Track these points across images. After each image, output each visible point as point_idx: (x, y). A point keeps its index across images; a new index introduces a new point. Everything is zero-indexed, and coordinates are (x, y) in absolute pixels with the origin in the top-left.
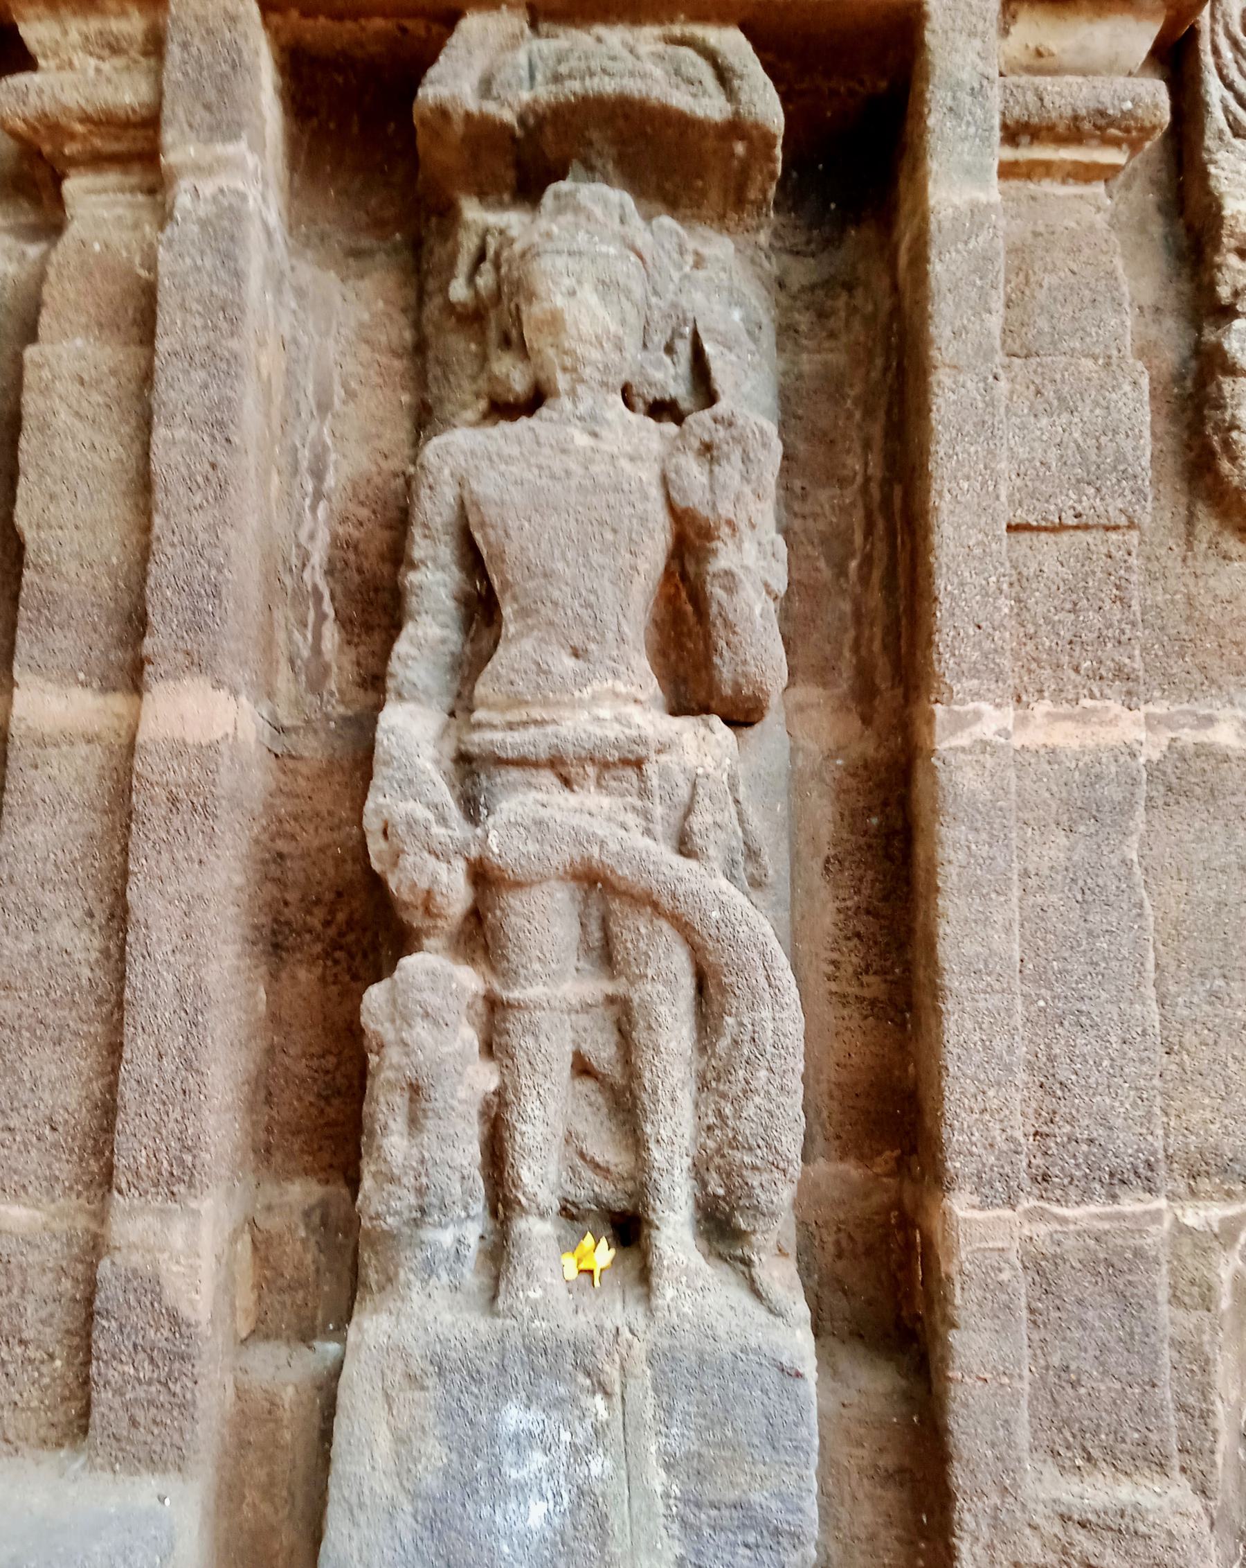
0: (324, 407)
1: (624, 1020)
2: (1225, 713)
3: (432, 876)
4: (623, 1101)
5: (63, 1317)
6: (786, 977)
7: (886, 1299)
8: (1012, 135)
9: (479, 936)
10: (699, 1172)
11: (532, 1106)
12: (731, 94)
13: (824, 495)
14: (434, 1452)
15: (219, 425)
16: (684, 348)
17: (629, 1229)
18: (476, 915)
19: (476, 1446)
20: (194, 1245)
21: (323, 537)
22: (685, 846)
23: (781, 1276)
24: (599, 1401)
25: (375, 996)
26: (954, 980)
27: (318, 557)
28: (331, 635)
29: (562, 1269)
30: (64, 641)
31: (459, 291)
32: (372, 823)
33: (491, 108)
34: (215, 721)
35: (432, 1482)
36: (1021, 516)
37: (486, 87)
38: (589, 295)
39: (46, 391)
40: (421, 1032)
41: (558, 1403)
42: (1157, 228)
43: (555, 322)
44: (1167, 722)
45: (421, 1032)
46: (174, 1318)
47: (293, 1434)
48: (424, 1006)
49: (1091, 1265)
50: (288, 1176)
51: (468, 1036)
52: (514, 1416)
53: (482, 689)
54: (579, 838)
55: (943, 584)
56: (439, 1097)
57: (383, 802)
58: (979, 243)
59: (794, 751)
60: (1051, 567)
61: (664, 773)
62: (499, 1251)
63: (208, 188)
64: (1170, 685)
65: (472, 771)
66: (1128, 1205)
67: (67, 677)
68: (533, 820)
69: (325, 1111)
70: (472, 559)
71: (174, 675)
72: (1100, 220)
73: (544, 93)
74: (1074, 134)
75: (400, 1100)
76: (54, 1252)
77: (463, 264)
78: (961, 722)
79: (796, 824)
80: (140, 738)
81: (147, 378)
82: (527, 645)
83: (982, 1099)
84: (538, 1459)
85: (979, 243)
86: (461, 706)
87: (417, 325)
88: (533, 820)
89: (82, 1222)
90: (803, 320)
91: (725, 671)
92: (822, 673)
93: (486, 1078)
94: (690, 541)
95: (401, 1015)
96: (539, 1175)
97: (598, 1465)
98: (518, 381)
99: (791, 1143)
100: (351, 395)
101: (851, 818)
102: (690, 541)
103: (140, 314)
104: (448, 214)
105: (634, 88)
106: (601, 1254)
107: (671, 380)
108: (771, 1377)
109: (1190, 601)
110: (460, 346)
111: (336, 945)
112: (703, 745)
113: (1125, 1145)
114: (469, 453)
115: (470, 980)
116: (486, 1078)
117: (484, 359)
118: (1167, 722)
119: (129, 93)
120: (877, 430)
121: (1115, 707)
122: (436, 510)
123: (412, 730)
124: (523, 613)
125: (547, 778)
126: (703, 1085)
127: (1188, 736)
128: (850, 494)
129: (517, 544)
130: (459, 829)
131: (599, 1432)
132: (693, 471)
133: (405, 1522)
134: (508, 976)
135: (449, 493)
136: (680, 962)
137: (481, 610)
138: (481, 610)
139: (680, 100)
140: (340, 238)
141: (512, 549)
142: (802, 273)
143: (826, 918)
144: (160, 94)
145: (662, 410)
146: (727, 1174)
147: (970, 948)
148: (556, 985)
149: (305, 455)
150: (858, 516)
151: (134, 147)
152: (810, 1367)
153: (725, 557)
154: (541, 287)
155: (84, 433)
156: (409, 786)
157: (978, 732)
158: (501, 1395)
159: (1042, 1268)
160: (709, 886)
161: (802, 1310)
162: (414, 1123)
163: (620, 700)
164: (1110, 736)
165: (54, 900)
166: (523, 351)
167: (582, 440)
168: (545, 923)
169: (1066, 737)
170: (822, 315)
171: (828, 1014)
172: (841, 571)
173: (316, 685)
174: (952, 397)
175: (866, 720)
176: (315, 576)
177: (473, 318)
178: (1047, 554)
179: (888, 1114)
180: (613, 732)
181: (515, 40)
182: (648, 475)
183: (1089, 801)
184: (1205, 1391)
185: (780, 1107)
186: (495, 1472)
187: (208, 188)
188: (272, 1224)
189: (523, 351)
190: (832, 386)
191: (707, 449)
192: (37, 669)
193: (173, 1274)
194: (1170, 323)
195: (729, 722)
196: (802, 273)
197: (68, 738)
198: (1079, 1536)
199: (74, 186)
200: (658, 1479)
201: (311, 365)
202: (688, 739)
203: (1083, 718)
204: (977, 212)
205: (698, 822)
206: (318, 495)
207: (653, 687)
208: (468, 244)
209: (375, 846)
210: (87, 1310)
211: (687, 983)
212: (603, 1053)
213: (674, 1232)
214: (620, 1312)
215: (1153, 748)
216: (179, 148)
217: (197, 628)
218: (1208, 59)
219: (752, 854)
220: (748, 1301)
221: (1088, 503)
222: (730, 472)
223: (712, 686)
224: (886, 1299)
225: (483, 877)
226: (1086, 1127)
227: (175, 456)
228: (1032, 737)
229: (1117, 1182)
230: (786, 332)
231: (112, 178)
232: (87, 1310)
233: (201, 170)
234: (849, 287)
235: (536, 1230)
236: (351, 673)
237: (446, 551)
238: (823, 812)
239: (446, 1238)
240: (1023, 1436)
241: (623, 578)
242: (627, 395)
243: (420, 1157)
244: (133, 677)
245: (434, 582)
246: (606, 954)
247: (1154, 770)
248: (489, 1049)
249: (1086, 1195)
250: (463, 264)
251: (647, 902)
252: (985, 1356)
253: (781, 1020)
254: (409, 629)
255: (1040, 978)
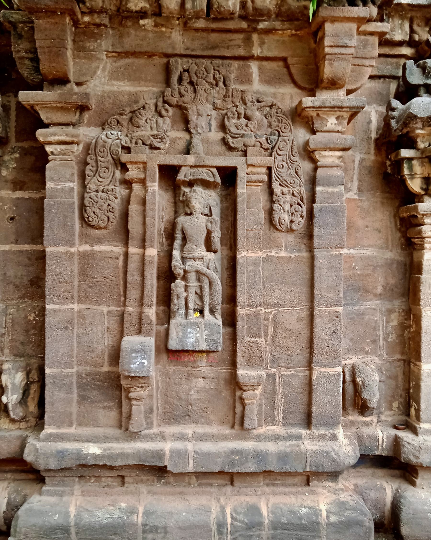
0: (163, 210)
1: (201, 288)
2: (273, 251)
3: (180, 271)
4: (201, 297)
5: (137, 321)
6: (220, 283)
7: (231, 320)
8: (248, 182)
9: (184, 278)
10: (209, 305)
11: (190, 297)
12: (214, 178)
13: (226, 222)
14: (181, 334)
15: (154, 218)
16: (208, 207)
17: (201, 312)
18: (184, 275)
19: (185, 333)
20: (151, 312)
21: (163, 227)
22: (208, 268)
23: (219, 317)
24: (198, 329)
25: (173, 285)
26: (239, 283)
27: (163, 230)
28: (164, 240)
29: (194, 316)
30: (135, 242)
31: (181, 198)
32: (172, 265)
33: (186, 179)
34: (153, 252)
35: (180, 337)
36: (248, 229)
37: (185, 176)
38: (197, 203)
39: (132, 212)
40: (178, 289)
41: (194, 329)
42: (267, 190)
43: (193, 206)
44: (266, 252)
45: (178, 289)
46: (151, 320)
47: (163, 335)
48: (178, 286)
49: (253, 315)
50: (160, 306)
51: (183, 289)
52: (189, 330)
53: (184, 249)
54: (196, 267)
55: (238, 238)
56: (180, 296)
57: (174, 263)
58: (243, 197)
59: (222, 255)
60: (252, 235)
61: (206, 260)
62: (187, 314)
63: (152, 189)
64: (267, 248)
65: (183, 259)
66: (258, 309)
67: (135, 246)
68: (191, 265)
69: (166, 299)
70: (183, 233)
71: (149, 247)
72: (259, 191)
73: (191, 177)
74: (255, 182)
75: (176, 296)
76: (135, 313)
77: (181, 195)
78: (240, 254)
79: (222, 265)
80: (145, 255)
81: (144, 211)
82: (190, 245)
83: (242, 297)
84: (192, 335)
85: (243, 197)
86: (182, 250)
87: (175, 199)
88: (191, 265)
89: (139, 310)
90: (224, 199)
91: (213, 248)
92: (226, 245)
93: (185, 294)
94: (209, 233)
95: (176, 287)
96: (191, 305)
97: (198, 335)
98: (189, 212)
99: (220, 301)
100: (166, 209)
101: (229, 263)
102: (209, 233)
103: (144, 202)
104: (179, 188)
105: (203, 177)
106: (198, 314)
107: (207, 211)
108: (217, 326)
109: (270, 237)
110: (181, 205)
111: (165, 278)
112: (210, 256)
113: (258, 302)
114: (182, 219)
115: (183, 283)
116: (185, 294)
117: (184, 207)
118: (266, 252)
119: (142, 176)
120: (233, 214)
121: (259, 251)
122: (179, 227)
123: (176, 253)
124: (190, 241)
125: (192, 260)
126: (210, 295)
127: (269, 254)
128: (229, 222)
129: (189, 232)
130: (182, 266)
131: (198, 332)
132: (209, 225)
133: (178, 341)
134: (188, 283)
135: (181, 226)
136: (207, 281)
137: (184, 239)
138: (184, 239)
139: (208, 179)
140: (165, 187)
141: (188, 234)
142: (224, 193)
143: (226, 275)
144: (146, 176)
145: (206, 215)
146: (213, 305)
147: (240, 280)
148: (193, 284)
149: (161, 217)
150: (230, 226)
151: (143, 182)
152: (221, 325)
153: (213, 235)
154: (192, 202)
155: (137, 217)
156: (177, 261)
157: (242, 255)
158: (188, 328)
159: (247, 315)
160: (211, 273)
161: (221, 320)
162: (178, 299)
163: (201, 251)
164: (258, 255)
165: (135, 273)
166: (189, 208)
167: (196, 220)
168: (192, 277)
169: (253, 255)
170: (226, 199)
171: (225, 287)
172: (228, 232)
173: (162, 246)
174: (240, 215)
175: (231, 251)
176: (162, 232)
177: (183, 202)
178: (251, 233)
179: (231, 299)
180: (200, 255)
181: (188, 170)
182: (204, 225)
183: (255, 263)
184: (267, 330)
185: (219, 297)
186: (187, 336)
187: (152, 189)
188: (158, 312)
189: (189, 208)
190: (227, 208)
191: (211, 222)
192: (132, 246)
193: (150, 315)
194: (268, 202)
195: (214, 252)
196: (224, 193)
197: (135, 254)
198: (251, 344)
199: (133, 185)
200: (205, 337)
201: (299, 533)
202: (209, 255)
203: (255, 253)
204: (243, 193)
205: (210, 265)
206: (163, 222)
207: (205, 249)
208: (182, 193)
209: (173, 268)
210: (140, 319)
211: (208, 284)
212: (199, 291)
213: (207, 312)
214: (201, 319)
215: (265, 255)
216: (148, 184)
217: (152, 242)
218: (273, 171)
219: (216, 268)
220: (214, 319)
221: (256, 227)
222: (214, 225)
223: (212, 249)
224: (231, 320)
225: (185, 271)
226: (254, 300)
227: (149, 221)
228: (249, 255)
229: (257, 306)
230: (222, 201)
231: (138, 184)
232: (140, 319)
233: (151, 186)
234: (230, 195)
235: (191, 311)
236: (167, 244)
237: (180, 232)
238: (225, 262)
239: (181, 312)
240: (245, 333)
241: (201, 237)
242: (202, 214)
243: (178, 303)
244: (144, 247)
245: (179, 235)
246: (199, 280)
247: (265, 258)
248: (185, 291)
249: (253, 308)
250: (181, 195)
251: (204, 274)
252: (241, 325)
253: (219, 287)
254: (176, 241)
255: (249, 283)
